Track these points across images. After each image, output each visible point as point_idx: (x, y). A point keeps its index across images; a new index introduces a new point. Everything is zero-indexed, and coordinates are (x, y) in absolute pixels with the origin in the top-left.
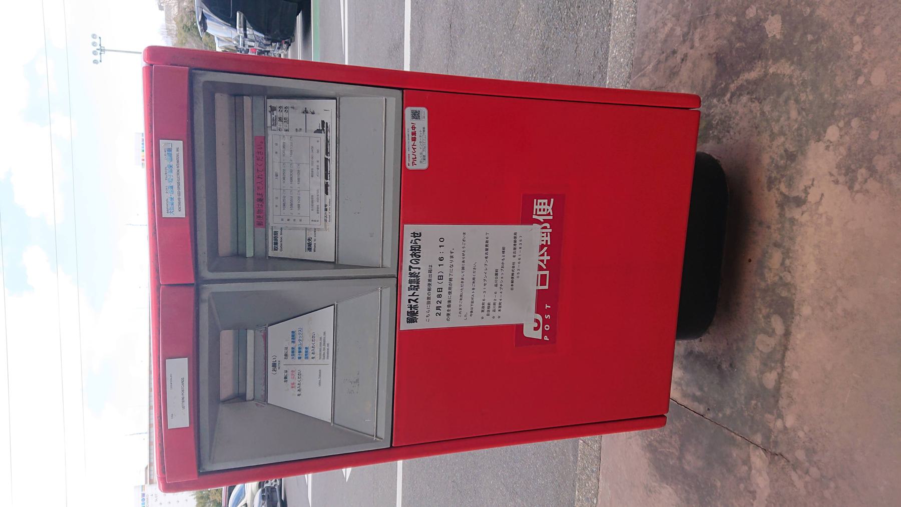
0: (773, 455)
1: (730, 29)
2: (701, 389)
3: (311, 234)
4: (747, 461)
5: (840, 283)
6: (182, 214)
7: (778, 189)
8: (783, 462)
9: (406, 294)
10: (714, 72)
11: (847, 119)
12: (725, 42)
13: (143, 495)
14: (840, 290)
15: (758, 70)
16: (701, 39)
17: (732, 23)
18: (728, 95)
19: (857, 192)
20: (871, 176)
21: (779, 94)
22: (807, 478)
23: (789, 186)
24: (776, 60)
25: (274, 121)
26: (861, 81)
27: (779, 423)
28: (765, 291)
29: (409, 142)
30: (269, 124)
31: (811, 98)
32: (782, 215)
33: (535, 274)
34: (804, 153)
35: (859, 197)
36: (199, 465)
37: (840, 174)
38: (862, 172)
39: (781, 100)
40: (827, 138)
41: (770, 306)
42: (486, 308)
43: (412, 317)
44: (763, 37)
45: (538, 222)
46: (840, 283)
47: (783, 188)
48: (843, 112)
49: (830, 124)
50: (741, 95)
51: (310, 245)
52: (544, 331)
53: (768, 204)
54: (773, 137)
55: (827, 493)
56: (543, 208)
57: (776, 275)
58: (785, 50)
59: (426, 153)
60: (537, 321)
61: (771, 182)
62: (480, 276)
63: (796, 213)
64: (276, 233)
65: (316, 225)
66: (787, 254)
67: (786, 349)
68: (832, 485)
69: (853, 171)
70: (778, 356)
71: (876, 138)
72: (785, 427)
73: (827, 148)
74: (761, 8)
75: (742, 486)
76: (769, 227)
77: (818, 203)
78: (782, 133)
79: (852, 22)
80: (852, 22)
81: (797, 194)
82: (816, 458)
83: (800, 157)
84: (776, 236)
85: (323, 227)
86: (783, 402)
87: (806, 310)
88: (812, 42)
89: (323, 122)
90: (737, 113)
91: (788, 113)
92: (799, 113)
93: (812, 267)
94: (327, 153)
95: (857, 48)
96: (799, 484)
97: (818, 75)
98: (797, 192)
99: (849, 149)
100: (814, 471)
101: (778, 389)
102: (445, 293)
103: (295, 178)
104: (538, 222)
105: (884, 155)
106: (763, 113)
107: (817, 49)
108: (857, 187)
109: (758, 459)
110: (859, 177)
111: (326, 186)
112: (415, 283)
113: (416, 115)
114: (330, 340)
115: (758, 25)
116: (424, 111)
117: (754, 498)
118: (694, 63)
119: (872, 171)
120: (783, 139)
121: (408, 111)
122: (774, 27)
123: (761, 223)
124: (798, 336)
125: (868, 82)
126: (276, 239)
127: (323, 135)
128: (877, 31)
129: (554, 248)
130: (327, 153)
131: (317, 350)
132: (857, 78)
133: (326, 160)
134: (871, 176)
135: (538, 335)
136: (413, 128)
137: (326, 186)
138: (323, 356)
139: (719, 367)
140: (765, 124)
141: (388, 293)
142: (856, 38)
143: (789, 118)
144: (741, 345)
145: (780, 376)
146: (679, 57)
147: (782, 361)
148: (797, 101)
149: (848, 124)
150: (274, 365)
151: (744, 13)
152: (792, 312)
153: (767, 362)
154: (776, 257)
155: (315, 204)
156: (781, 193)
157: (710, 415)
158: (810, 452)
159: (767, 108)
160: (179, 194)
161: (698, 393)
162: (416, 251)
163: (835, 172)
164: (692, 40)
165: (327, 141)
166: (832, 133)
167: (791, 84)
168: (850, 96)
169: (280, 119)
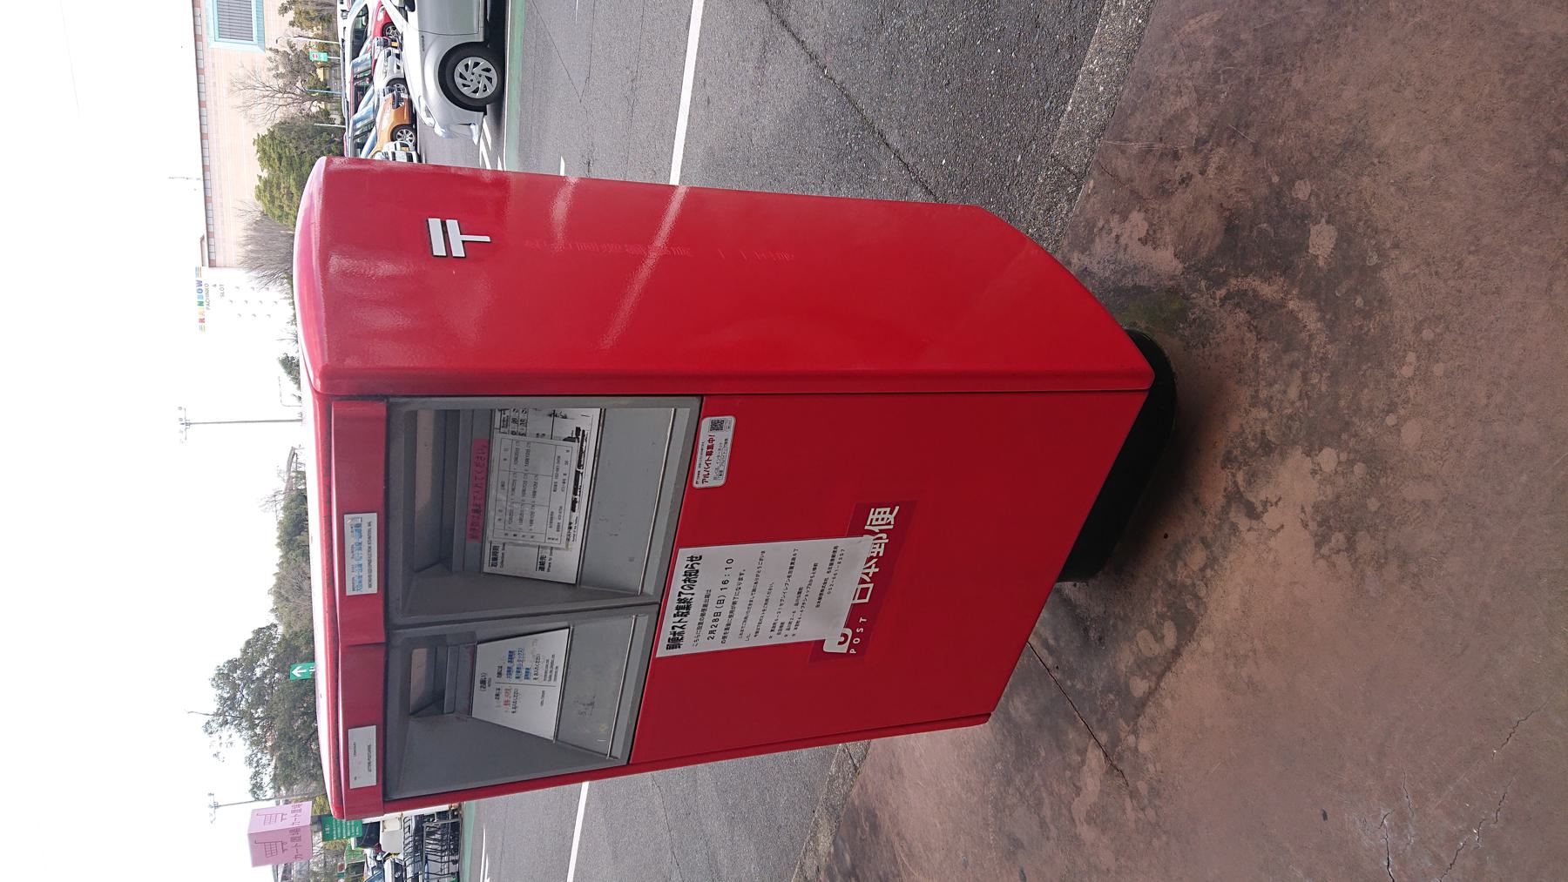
0: (1113, 766)
1: (1263, 190)
2: (1056, 639)
3: (546, 553)
4: (1082, 752)
5: (1258, 644)
6: (374, 590)
7: (1234, 475)
8: (1121, 781)
9: (669, 621)
10: (1218, 241)
11: (1352, 456)
12: (1250, 204)
13: (200, 283)
14: (1254, 651)
15: (1275, 287)
16: (1220, 169)
17: (1271, 185)
18: (1223, 292)
19: (1323, 556)
20: (1347, 550)
21: (1288, 348)
22: (1141, 815)
23: (1252, 478)
24: (1303, 296)
25: (505, 423)
26: (1391, 420)
27: (1131, 739)
28: (1171, 586)
29: (701, 457)
30: (497, 424)
31: (1324, 389)
32: (1225, 510)
33: (855, 586)
34: (1283, 455)
35: (1322, 563)
36: (385, 795)
37: (1313, 519)
38: (1338, 539)
39: (1287, 359)
40: (1318, 459)
41: (1169, 607)
42: (777, 627)
43: (675, 642)
44: (1302, 246)
45: (872, 533)
46: (1258, 644)
47: (1240, 477)
48: (1352, 443)
49: (1329, 445)
50: (1238, 305)
51: (542, 564)
52: (851, 646)
53: (1216, 484)
54: (1255, 401)
55: (1155, 843)
56: (882, 517)
57: (1188, 576)
58: (1318, 289)
59: (724, 468)
60: (845, 636)
61: (1228, 460)
62: (776, 595)
63: (1243, 522)
64: (496, 548)
65: (555, 544)
66: (1212, 561)
67: (1168, 668)
68: (1164, 838)
69: (1330, 527)
70: (1158, 669)
71: (1373, 509)
72: (1136, 750)
73: (1314, 472)
74: (1318, 196)
75: (1068, 773)
76: (1204, 514)
77: (1274, 532)
78: (1268, 405)
79: (1418, 330)
80: (1418, 330)
81: (1253, 500)
82: (1157, 803)
83: (1276, 456)
84: (1207, 530)
85: (563, 546)
86: (1143, 721)
87: (1207, 644)
88: (1359, 311)
89: (578, 429)
90: (1224, 327)
91: (1288, 385)
92: (1300, 398)
93: (1234, 601)
94: (580, 465)
95: (1407, 371)
96: (1131, 815)
97: (1346, 364)
98: (1257, 497)
99: (1338, 497)
100: (1151, 812)
101: (1142, 704)
102: (723, 619)
103: (529, 491)
104: (872, 533)
105: (1372, 537)
106: (1256, 357)
107: (1361, 327)
108: (1325, 550)
109: (1095, 758)
110: (1333, 544)
111: (574, 502)
112: (684, 607)
113: (716, 426)
114: (560, 662)
115: (1302, 220)
116: (730, 421)
117: (1078, 795)
118: (1196, 200)
119: (1351, 545)
120: (1265, 414)
121: (706, 423)
122: (1322, 241)
123: (1196, 501)
124: (1187, 665)
125: (1397, 429)
126: (495, 553)
127: (576, 445)
128: (1438, 369)
129: (886, 565)
130: (580, 465)
131: (541, 672)
132: (1388, 412)
133: (577, 473)
134: (1347, 550)
135: (843, 649)
136: (711, 440)
137: (574, 502)
138: (549, 677)
139: (1086, 630)
140: (1252, 374)
141: (644, 621)
142: (1411, 357)
143: (1285, 392)
144: (1120, 625)
145: (1151, 692)
146: (1179, 172)
147: (1160, 677)
148: (1305, 378)
149: (1351, 463)
150: (483, 682)
151: (1292, 183)
152: (1191, 633)
153: (1142, 665)
154: (1198, 557)
155: (555, 521)
156: (1235, 483)
157: (1058, 675)
158: (1154, 792)
159: (1264, 356)
160: (370, 571)
161: (1051, 642)
162: (691, 576)
163: (1309, 509)
164: (1207, 158)
165: (581, 452)
166: (1328, 458)
167: (1308, 348)
168: (1370, 430)
169: (514, 421)
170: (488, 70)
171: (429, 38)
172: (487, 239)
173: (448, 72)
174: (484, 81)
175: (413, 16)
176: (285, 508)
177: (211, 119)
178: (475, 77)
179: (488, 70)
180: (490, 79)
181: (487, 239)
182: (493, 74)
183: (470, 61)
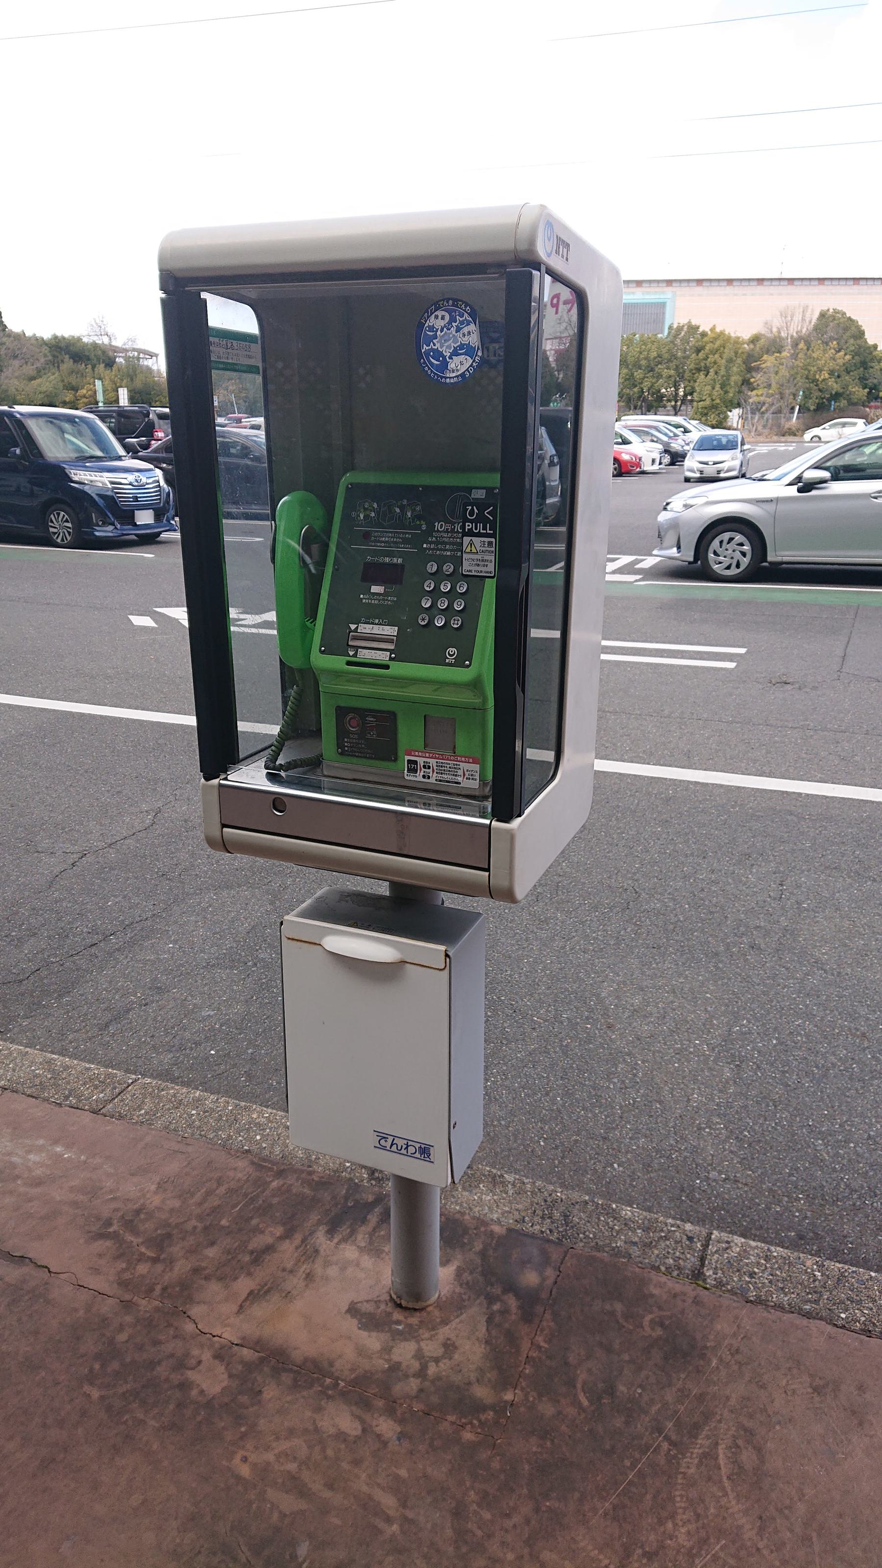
84: (81, 1313)
170: (738, 566)
171: (771, 507)
172: (743, 651)
173: (743, 527)
174: (727, 561)
175: (793, 491)
176: (95, 346)
177: (774, 289)
178: (730, 553)
179: (738, 566)
180: (728, 568)
181: (743, 651)
182: (734, 571)
183: (746, 548)
